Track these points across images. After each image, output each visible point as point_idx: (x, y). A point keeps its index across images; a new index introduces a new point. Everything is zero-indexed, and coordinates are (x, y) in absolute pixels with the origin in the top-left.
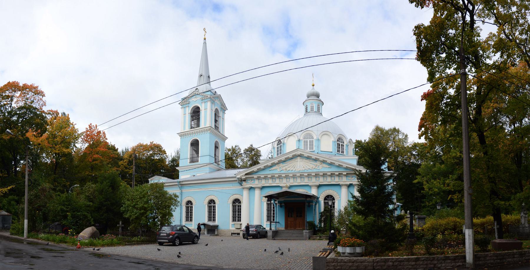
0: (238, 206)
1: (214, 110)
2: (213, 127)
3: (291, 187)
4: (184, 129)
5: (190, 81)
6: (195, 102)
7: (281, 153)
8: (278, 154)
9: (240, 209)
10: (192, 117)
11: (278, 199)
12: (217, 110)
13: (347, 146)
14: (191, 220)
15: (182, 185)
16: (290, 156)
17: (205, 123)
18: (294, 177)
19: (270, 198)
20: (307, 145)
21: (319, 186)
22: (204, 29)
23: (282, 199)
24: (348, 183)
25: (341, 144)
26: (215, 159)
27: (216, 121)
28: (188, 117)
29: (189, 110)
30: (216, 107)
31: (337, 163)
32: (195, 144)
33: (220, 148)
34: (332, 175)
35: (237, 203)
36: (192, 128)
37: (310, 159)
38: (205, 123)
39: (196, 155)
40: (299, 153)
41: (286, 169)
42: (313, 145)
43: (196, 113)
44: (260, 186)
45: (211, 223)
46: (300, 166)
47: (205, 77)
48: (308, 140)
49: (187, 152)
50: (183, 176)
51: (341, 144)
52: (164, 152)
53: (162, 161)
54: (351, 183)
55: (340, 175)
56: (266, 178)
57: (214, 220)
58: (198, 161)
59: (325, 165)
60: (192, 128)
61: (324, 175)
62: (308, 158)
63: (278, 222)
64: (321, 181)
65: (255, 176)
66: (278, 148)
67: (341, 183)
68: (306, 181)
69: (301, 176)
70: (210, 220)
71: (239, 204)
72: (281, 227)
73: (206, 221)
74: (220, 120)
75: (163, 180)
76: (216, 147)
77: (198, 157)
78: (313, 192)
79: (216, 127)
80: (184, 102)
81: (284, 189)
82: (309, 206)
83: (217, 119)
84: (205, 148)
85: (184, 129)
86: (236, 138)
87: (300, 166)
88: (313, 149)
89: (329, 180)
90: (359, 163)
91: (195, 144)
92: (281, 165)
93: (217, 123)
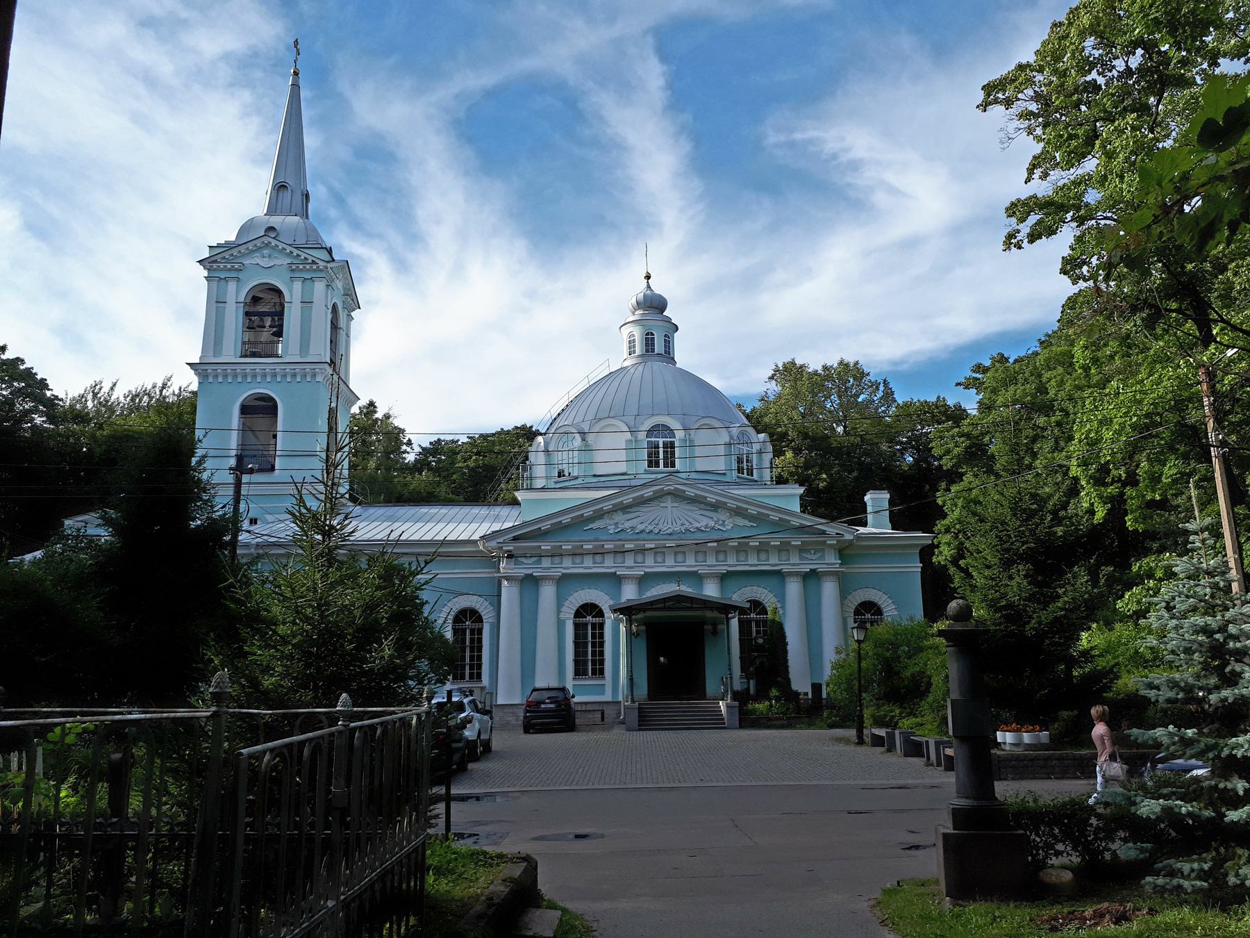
1: (330, 307)
6: (266, 269)
12: (334, 307)
17: (305, 345)
18: (658, 551)
28: (234, 318)
29: (236, 294)
37: (700, 503)
41: (633, 528)
44: (557, 572)
55: (784, 548)
56: (577, 554)
64: (732, 563)
65: (546, 546)
67: (786, 569)
68: (690, 563)
69: (679, 550)
71: (477, 626)
80: (220, 263)
82: (715, 633)
87: (670, 518)
88: (673, 465)
89: (752, 562)
91: (260, 410)
92: (619, 517)
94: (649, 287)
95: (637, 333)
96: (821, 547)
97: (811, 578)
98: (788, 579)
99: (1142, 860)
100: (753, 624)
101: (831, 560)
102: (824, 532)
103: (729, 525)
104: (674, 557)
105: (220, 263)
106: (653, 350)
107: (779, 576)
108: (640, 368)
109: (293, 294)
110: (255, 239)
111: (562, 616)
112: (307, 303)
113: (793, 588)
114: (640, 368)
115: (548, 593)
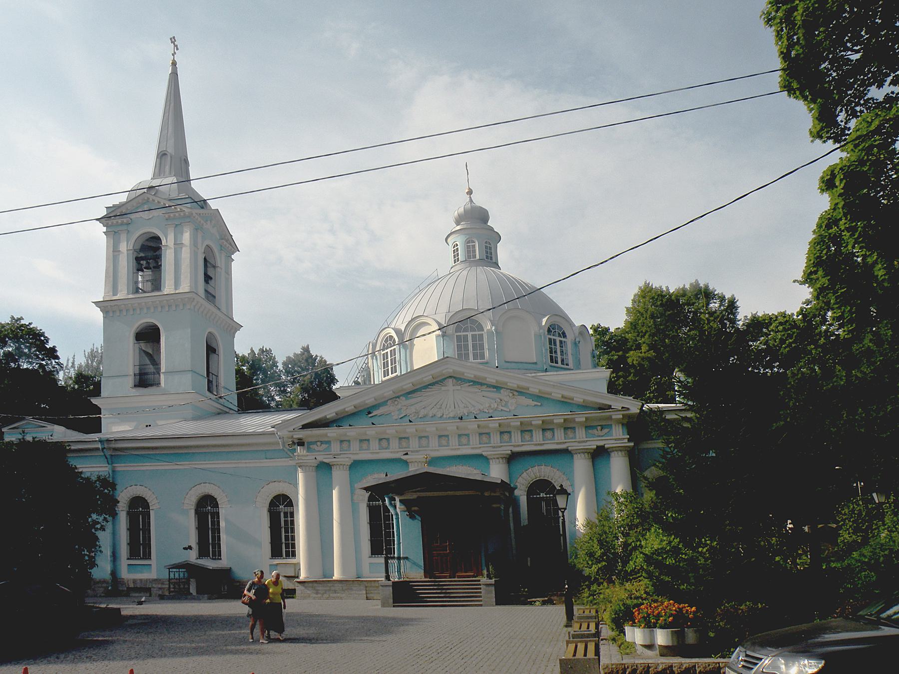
0: (286, 514)
1: (201, 249)
2: (201, 292)
3: (432, 461)
4: (115, 291)
5: (130, 172)
6: (147, 224)
7: (394, 370)
8: (386, 373)
9: (292, 522)
10: (138, 259)
11: (400, 494)
13: (576, 344)
14: (147, 556)
15: (115, 451)
16: (428, 379)
17: (177, 284)
19: (377, 492)
20: (466, 346)
21: (512, 458)
22: (173, 40)
23: (410, 496)
24: (593, 445)
25: (558, 339)
26: (210, 382)
27: (208, 278)
28: (125, 263)
30: (208, 242)
31: (557, 394)
32: (149, 336)
33: (221, 351)
34: (546, 427)
35: (280, 510)
36: (137, 290)
37: (482, 384)
38: (177, 284)
39: (151, 368)
40: (450, 369)
42: (482, 347)
43: (149, 255)
45: (209, 564)
46: (454, 400)
47: (173, 157)
48: (470, 334)
49: (128, 357)
50: (114, 427)
51: (558, 339)
52: (52, 353)
53: (50, 377)
54: (601, 443)
55: (568, 427)
57: (217, 555)
58: (158, 384)
59: (523, 400)
60: (137, 290)
61: (526, 429)
62: (476, 383)
63: (407, 558)
64: (518, 443)
66: (385, 356)
67: (572, 446)
70: (203, 553)
71: (288, 509)
72: (415, 573)
73: (192, 557)
74: (219, 276)
75: (58, 433)
76: (211, 350)
77: (158, 371)
78: (496, 473)
79: (210, 296)
80: (115, 219)
81: (414, 469)
83: (210, 273)
84: (177, 351)
85: (115, 291)
86: (266, 319)
88: (483, 357)
89: (537, 442)
90: (612, 388)
92: (403, 401)
93: (211, 282)
94: (471, 201)
95: (459, 240)
96: (605, 425)
97: (599, 454)
98: (612, 454)
99: (823, 667)
100: (543, 504)
101: (618, 437)
102: (610, 407)
103: (534, 413)
104: (463, 444)
105: (115, 219)
106: (475, 256)
107: (566, 453)
108: (465, 273)
109: (168, 241)
110: (144, 199)
111: (355, 497)
112: (178, 245)
113: (581, 466)
114: (465, 273)
115: (339, 476)
